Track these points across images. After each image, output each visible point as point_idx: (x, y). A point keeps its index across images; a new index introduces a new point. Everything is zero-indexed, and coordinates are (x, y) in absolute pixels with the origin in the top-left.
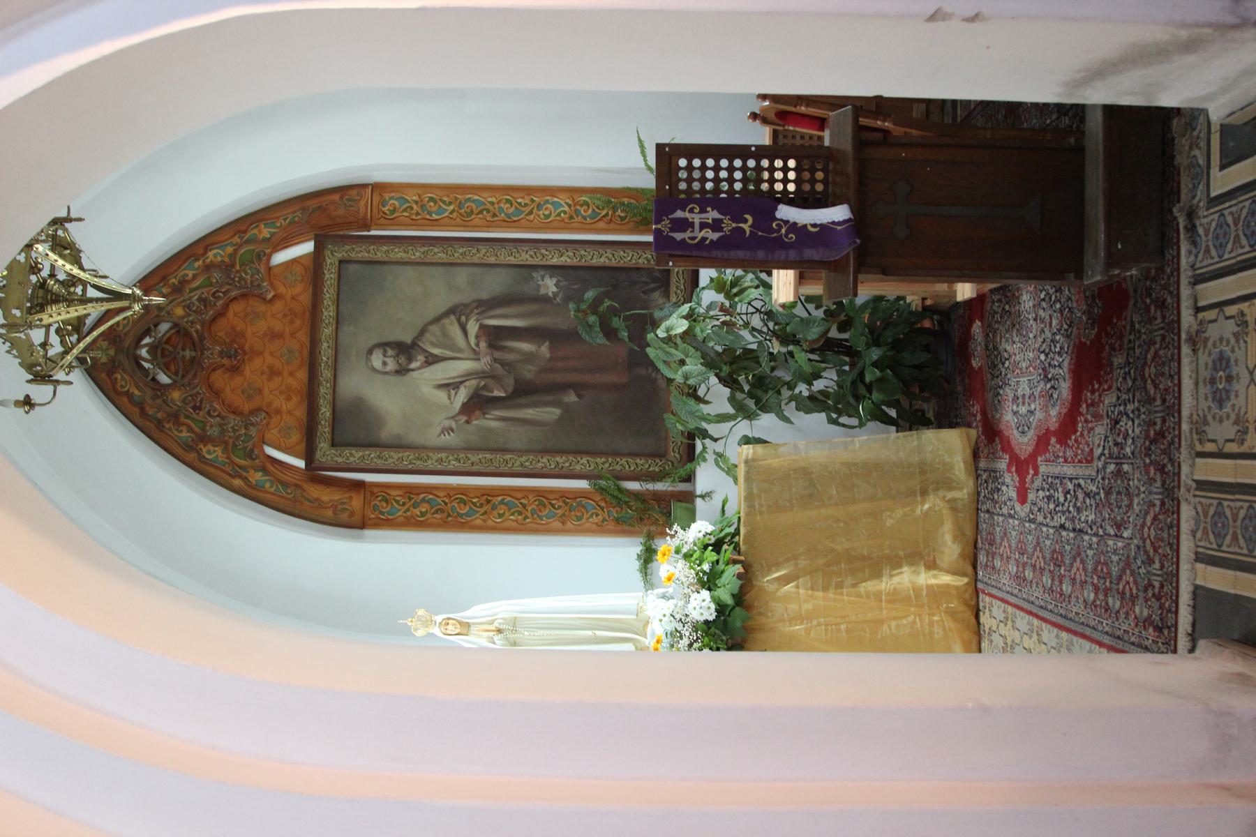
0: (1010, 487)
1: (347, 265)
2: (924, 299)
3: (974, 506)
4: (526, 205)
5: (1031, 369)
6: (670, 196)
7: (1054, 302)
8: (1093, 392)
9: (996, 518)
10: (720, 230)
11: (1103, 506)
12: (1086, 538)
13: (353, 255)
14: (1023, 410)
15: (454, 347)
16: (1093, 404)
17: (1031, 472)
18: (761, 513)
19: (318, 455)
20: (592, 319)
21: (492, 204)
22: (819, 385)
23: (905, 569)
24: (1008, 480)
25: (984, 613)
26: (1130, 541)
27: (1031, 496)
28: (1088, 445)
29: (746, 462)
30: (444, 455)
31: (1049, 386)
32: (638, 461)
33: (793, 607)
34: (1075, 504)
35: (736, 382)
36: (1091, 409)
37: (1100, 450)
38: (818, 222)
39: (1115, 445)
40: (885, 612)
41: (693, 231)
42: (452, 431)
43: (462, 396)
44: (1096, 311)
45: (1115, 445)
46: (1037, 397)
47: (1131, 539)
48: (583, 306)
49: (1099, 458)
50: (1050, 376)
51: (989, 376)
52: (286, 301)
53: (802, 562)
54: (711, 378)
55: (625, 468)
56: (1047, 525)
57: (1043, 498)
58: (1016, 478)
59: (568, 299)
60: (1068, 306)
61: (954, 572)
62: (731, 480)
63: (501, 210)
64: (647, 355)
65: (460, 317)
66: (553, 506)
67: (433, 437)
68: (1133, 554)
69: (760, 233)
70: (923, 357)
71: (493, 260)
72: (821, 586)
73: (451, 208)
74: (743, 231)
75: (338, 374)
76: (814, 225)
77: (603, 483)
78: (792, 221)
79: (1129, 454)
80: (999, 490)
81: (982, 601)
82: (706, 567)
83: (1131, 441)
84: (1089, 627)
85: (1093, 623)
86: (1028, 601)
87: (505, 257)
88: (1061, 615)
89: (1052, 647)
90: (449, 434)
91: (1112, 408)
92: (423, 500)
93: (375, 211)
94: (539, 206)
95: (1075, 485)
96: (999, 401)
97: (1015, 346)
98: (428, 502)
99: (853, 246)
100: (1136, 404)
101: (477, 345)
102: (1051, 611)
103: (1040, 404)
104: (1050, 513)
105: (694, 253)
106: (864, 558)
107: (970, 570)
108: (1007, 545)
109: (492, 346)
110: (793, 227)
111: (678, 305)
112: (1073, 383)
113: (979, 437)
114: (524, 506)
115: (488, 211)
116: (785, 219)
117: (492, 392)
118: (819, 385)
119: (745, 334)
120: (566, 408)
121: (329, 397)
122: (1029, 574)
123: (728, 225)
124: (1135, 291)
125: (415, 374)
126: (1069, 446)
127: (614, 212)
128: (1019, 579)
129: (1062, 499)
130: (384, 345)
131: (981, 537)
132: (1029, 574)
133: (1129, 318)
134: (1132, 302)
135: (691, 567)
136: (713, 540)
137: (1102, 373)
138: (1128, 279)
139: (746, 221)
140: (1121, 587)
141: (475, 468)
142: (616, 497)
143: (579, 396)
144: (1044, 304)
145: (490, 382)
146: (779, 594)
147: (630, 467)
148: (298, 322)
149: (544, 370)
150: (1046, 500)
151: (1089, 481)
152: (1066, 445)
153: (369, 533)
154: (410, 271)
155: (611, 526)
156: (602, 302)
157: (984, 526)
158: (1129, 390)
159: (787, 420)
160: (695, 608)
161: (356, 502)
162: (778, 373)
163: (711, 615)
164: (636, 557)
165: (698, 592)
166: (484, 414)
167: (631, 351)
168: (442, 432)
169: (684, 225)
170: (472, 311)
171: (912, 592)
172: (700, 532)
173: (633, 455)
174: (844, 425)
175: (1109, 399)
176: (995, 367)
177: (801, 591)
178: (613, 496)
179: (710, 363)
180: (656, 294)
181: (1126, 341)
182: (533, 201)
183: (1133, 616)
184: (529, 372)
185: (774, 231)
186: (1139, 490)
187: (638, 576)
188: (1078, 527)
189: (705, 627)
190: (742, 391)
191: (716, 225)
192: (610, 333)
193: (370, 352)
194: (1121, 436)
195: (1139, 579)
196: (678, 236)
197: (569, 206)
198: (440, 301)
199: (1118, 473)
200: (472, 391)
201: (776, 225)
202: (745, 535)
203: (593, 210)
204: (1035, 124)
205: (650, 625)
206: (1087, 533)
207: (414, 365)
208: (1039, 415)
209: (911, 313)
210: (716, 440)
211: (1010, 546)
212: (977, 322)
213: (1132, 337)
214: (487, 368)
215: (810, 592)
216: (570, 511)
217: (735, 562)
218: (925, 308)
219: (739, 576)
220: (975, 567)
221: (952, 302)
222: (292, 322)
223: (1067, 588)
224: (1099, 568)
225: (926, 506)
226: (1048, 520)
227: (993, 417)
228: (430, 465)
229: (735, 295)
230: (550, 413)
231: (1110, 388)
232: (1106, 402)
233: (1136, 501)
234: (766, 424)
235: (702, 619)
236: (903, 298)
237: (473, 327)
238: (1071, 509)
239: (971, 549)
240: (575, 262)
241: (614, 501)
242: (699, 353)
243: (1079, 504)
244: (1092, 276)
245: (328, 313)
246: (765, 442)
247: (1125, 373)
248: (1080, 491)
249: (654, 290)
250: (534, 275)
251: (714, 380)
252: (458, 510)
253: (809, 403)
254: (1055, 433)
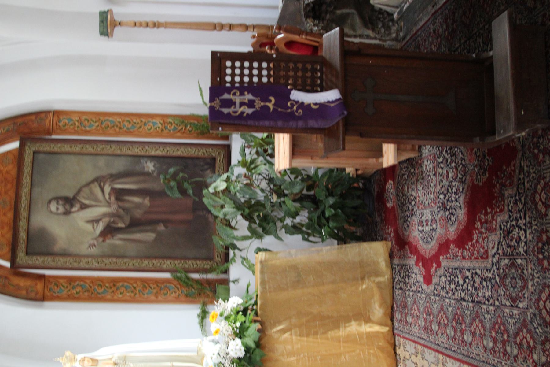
0: (418, 275)
2: (357, 170)
3: (391, 286)
4: (138, 123)
5: (433, 204)
6: (220, 84)
7: (450, 163)
8: (486, 214)
9: (407, 293)
10: (253, 107)
11: (499, 287)
12: (484, 307)
13: (41, 149)
14: (427, 229)
15: (97, 200)
16: (486, 222)
17: (435, 265)
18: (270, 292)
19: (18, 260)
20: (173, 183)
21: (120, 122)
22: (298, 220)
23: (353, 323)
24: (416, 270)
25: (399, 348)
26: (526, 310)
27: (435, 280)
28: (484, 248)
29: (261, 262)
30: (90, 260)
31: (447, 213)
32: (198, 262)
33: (289, 347)
34: (473, 286)
35: (252, 218)
36: (485, 225)
37: (494, 251)
38: (318, 102)
39: (508, 247)
40: (342, 348)
41: (235, 107)
42: (95, 246)
43: (100, 227)
44: (486, 164)
45: (508, 247)
46: (438, 220)
47: (527, 308)
48: (168, 177)
49: (494, 256)
50: (448, 207)
51: (400, 211)
52: (3, 174)
53: (294, 320)
54: (238, 216)
55: (190, 266)
56: (449, 298)
57: (445, 281)
58: (423, 270)
59: (159, 174)
60: (462, 164)
61: (381, 324)
62: (251, 273)
63: (124, 126)
64: (203, 203)
65: (100, 184)
66: (151, 288)
67: (84, 249)
68: (529, 318)
69: (279, 110)
70: (358, 202)
71: (119, 152)
72: (305, 334)
73: (97, 124)
74: (268, 108)
75: (31, 214)
76: (316, 104)
77: (178, 274)
78: (300, 101)
79: (522, 252)
80: (409, 277)
81: (398, 340)
82: (238, 325)
83: (523, 244)
84: (490, 364)
85: (493, 362)
86: (435, 344)
87: (126, 151)
88: (464, 355)
89: (432, 363)
90: (93, 248)
91: (505, 224)
92: (78, 285)
93: (55, 125)
94: (145, 124)
95: (472, 273)
96: (407, 225)
97: (419, 192)
98: (81, 286)
99: (342, 117)
100: (528, 219)
101: (110, 198)
102: (454, 351)
103: (440, 225)
104: (452, 291)
105: (236, 122)
106: (329, 317)
107: (389, 322)
108: (417, 309)
109: (118, 199)
110: (301, 105)
111: (220, 175)
112: (468, 210)
113: (392, 246)
114: (135, 288)
115: (117, 126)
116: (296, 99)
117: (117, 224)
118: (298, 220)
119: (258, 191)
120: (159, 234)
121: (25, 227)
122: (435, 327)
123: (259, 104)
124: (523, 146)
125: (75, 215)
126: (466, 249)
127: (186, 127)
128: (427, 329)
129: (461, 282)
130: (57, 199)
131: (397, 304)
132: (435, 327)
133: (517, 165)
134: (520, 154)
136: (242, 308)
137: (494, 202)
138: (516, 140)
139: (270, 101)
140: (438, 320)
141: (107, 267)
142: (186, 283)
143: (166, 227)
144: (442, 165)
145: (116, 219)
146: (280, 339)
147: (193, 265)
148: (9, 186)
149: (146, 213)
150: (447, 282)
151: (485, 271)
152: (464, 248)
153: (47, 304)
154: (72, 157)
155: (183, 298)
156: (178, 174)
157: (399, 297)
158: (520, 211)
159: (280, 239)
160: (232, 350)
161: (40, 286)
162: (274, 214)
163: (242, 354)
164: (197, 316)
165: (234, 340)
166: (113, 237)
167: (194, 201)
168: (89, 247)
169: (229, 103)
170: (107, 180)
171: (357, 336)
172: (234, 303)
173: (196, 259)
174: (311, 242)
175: (501, 218)
176: (404, 205)
177: (294, 337)
178: (184, 282)
179: (238, 207)
180: (208, 171)
181: (515, 180)
182: (141, 121)
183: (531, 361)
184: (138, 214)
185: (288, 108)
186: (533, 276)
187: (198, 327)
188: (476, 299)
189: (238, 361)
190: (255, 223)
191: (251, 104)
192: (183, 192)
193: (50, 202)
194: (514, 241)
195: (536, 336)
196: (226, 111)
197: (162, 124)
198: (90, 175)
199: (513, 265)
200: (106, 224)
201: (291, 104)
202: (261, 306)
203: (174, 127)
204: (200, 265)
205: (205, 359)
206: (484, 303)
207: (74, 209)
208: (440, 231)
209: (350, 178)
210: (241, 250)
211: (419, 310)
212: (390, 181)
213: (522, 176)
214: (115, 211)
215: (299, 338)
216: (160, 290)
217: (255, 321)
218: (358, 176)
219: (259, 331)
220: (392, 319)
221: (379, 168)
222: (6, 185)
223: (468, 337)
224: (497, 326)
225: (364, 286)
226: (450, 295)
227: (403, 234)
228: (82, 265)
229: (252, 169)
230: (150, 236)
231: (502, 211)
232: (499, 219)
233: (530, 283)
234: (268, 241)
235: (236, 356)
236: (344, 170)
237: (107, 189)
238: (470, 288)
239: (390, 310)
240: (164, 153)
241: (185, 285)
242: (232, 202)
243: (476, 285)
244: (505, 132)
245: (26, 180)
246: (269, 251)
247: (516, 200)
248: (477, 276)
249: (207, 169)
250: (142, 160)
251: (240, 217)
252: (98, 290)
253: (292, 229)
254: (454, 242)
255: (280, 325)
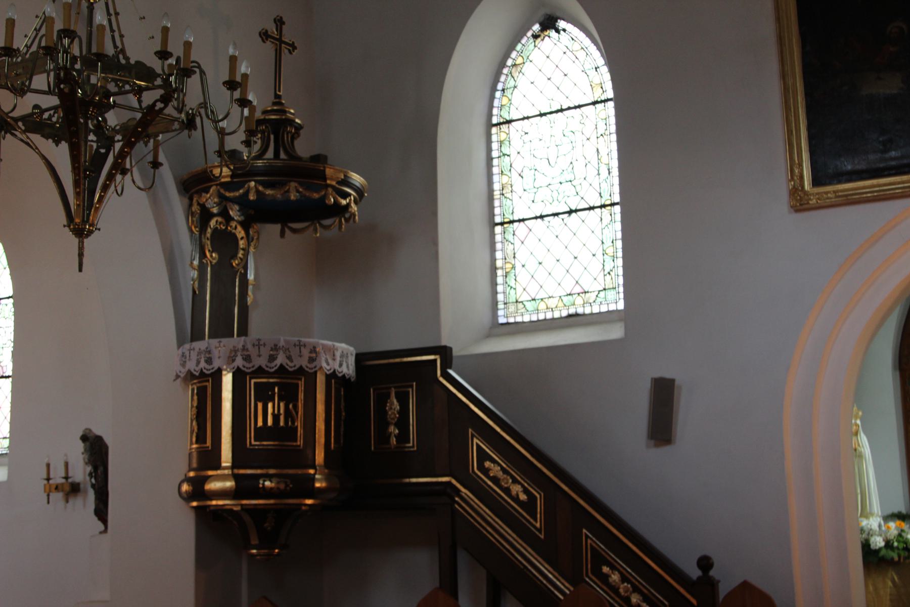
1: (904, 511)
135: (895, 537)
153: (898, 373)
163: (873, 546)
187: (889, 512)
217: (899, 557)
219: (892, 559)
255: (898, 579)
